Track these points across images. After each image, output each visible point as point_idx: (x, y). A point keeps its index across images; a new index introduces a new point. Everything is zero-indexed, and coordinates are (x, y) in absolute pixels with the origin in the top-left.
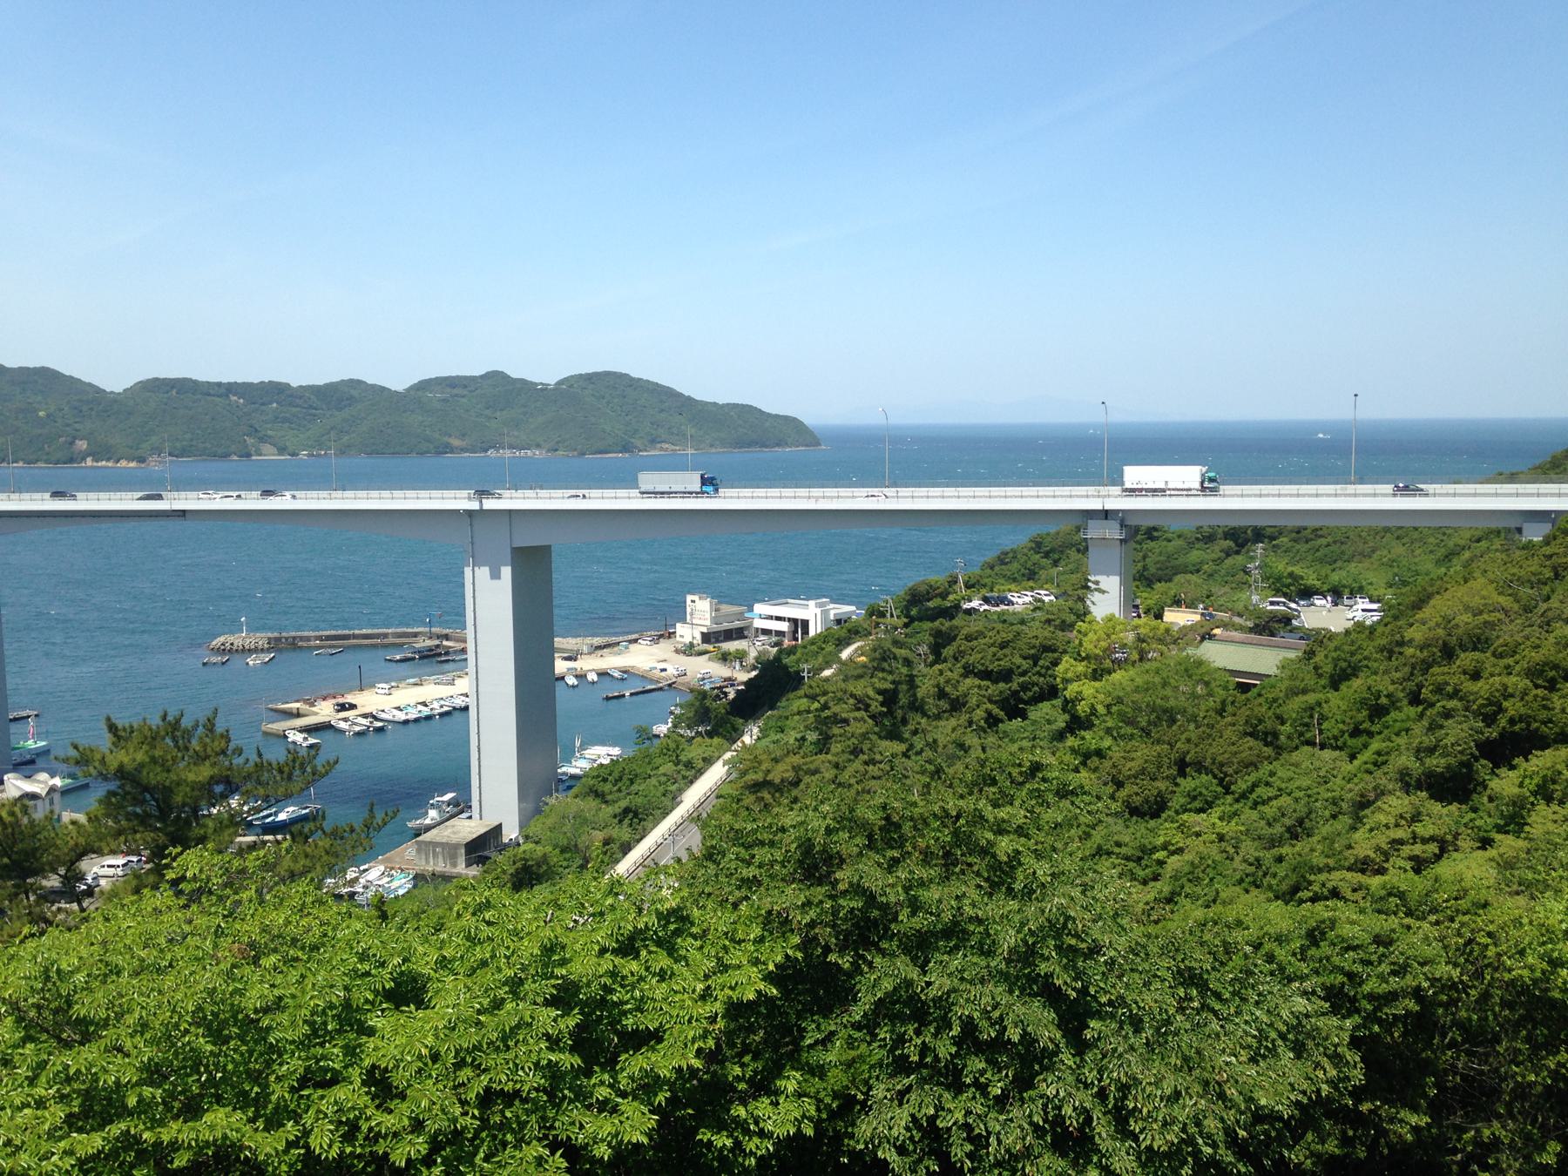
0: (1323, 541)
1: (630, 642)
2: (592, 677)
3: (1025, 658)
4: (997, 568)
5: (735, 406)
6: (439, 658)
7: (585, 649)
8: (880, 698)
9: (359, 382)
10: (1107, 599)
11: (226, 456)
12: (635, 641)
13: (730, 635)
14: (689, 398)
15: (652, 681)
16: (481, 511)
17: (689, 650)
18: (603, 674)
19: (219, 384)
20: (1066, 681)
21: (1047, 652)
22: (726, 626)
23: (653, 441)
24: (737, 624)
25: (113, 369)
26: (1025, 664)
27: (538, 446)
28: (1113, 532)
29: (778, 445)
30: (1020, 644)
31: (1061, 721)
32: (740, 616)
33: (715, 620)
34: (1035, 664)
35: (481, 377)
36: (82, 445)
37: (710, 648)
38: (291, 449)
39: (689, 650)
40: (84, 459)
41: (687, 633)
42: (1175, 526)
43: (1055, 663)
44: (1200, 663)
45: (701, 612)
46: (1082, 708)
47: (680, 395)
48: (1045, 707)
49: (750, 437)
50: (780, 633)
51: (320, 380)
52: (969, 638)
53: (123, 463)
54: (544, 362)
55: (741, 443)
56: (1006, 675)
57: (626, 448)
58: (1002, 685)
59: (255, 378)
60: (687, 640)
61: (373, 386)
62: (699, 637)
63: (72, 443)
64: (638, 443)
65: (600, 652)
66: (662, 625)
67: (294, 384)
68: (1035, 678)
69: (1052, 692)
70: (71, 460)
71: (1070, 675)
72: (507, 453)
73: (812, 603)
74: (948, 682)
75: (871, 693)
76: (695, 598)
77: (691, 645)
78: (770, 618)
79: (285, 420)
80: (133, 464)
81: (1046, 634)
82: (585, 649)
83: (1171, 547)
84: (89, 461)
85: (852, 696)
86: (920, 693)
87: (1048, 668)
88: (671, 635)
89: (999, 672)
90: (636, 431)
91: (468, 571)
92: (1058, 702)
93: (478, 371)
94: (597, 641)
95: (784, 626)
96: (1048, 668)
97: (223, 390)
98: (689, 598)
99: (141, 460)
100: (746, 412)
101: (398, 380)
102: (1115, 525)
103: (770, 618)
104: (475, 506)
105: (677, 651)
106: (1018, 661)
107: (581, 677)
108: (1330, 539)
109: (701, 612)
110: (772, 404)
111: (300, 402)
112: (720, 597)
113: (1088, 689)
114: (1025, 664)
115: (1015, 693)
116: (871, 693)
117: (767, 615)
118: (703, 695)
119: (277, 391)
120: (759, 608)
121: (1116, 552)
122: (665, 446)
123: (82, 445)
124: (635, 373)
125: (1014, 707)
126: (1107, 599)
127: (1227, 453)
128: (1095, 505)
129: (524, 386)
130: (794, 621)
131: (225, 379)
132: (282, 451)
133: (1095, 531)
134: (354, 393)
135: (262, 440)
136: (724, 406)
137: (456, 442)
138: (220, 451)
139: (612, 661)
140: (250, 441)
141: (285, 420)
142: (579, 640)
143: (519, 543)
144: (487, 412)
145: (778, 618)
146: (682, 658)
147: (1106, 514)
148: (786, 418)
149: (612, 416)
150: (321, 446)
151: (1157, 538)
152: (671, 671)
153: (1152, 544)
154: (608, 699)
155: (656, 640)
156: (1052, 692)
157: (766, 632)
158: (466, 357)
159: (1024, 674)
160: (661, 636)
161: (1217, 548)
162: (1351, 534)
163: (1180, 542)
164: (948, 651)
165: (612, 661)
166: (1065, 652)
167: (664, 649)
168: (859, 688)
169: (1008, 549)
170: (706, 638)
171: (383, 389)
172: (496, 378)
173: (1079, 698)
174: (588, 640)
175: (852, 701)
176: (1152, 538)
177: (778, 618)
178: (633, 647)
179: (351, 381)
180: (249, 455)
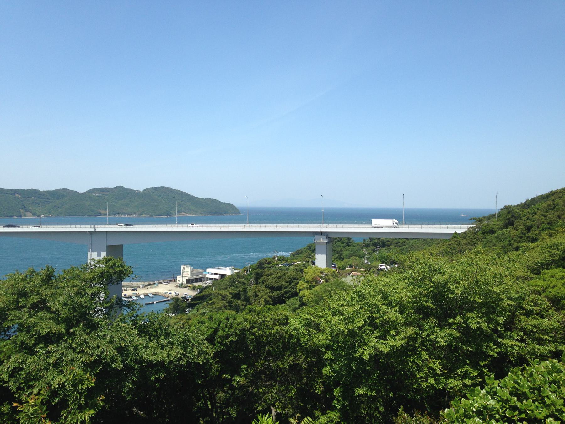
0: (405, 247)
1: (159, 283)
2: (142, 296)
3: (286, 282)
4: (296, 256)
5: (210, 199)
7: (141, 286)
8: (231, 296)
9: (67, 190)
10: (321, 261)
11: (12, 216)
12: (161, 283)
13: (197, 280)
14: (193, 196)
15: (165, 297)
16: (95, 232)
17: (181, 286)
18: (146, 295)
19: (12, 190)
20: (300, 290)
21: (294, 280)
22: (196, 277)
24: (200, 276)
25: (81, 186)
26: (287, 284)
27: (135, 213)
28: (324, 239)
29: (225, 214)
30: (285, 277)
31: (298, 304)
32: (201, 273)
33: (192, 275)
34: (290, 284)
35: (115, 188)
37: (189, 285)
38: (38, 214)
39: (181, 286)
41: (180, 280)
42: (357, 240)
43: (297, 284)
44: (342, 283)
45: (187, 272)
46: (304, 299)
47: (189, 195)
48: (293, 300)
49: (215, 209)
50: (216, 279)
51: (52, 189)
52: (268, 275)
54: (138, 183)
55: (211, 213)
56: (279, 288)
57: (168, 214)
58: (278, 292)
59: (26, 188)
60: (181, 282)
61: (72, 191)
62: (185, 281)
65: (146, 287)
66: (171, 275)
67: (41, 190)
68: (290, 289)
69: (296, 294)
71: (301, 288)
72: (123, 216)
73: (227, 268)
74: (258, 291)
75: (228, 294)
76: (185, 267)
77: (182, 284)
78: (212, 274)
79: (36, 203)
81: (294, 273)
82: (141, 286)
83: (355, 248)
85: (221, 295)
86: (248, 295)
87: (294, 286)
88: (175, 281)
89: (277, 287)
91: (89, 254)
92: (297, 298)
93: (113, 186)
94: (146, 283)
95: (217, 277)
96: (294, 286)
97: (13, 192)
98: (182, 267)
100: (214, 201)
101: (82, 189)
102: (324, 237)
103: (212, 274)
104: (93, 230)
105: (176, 286)
106: (284, 283)
107: (138, 296)
108: (407, 246)
109: (187, 272)
110: (223, 199)
111: (43, 197)
112: (194, 266)
113: (307, 293)
114: (287, 284)
115: (283, 295)
116: (228, 294)
117: (212, 273)
118: (177, 299)
119: (34, 193)
120: (209, 270)
121: (325, 247)
122: (183, 213)
124: (173, 187)
125: (280, 301)
126: (321, 261)
128: (318, 230)
129: (131, 191)
130: (221, 275)
131: (14, 188)
132: (34, 214)
133: (319, 239)
134: (65, 193)
135: (26, 211)
136: (206, 199)
137: (102, 212)
139: (151, 291)
140: (22, 211)
141: (36, 203)
142: (139, 283)
143: (108, 244)
144: (116, 201)
145: (215, 274)
146: (178, 289)
147: (322, 233)
148: (228, 204)
149: (164, 201)
150: (50, 213)
151: (350, 245)
152: (173, 293)
153: (349, 247)
154: (147, 304)
155: (169, 282)
156: (296, 294)
157: (211, 279)
158: (109, 181)
159: (286, 288)
160: (171, 281)
161: (370, 249)
162: (414, 244)
163: (358, 247)
164: (260, 280)
165: (151, 291)
166: (300, 280)
167: (172, 285)
168: (223, 292)
169: (299, 249)
170: (188, 281)
171: (76, 192)
172: (120, 189)
173: (304, 296)
174: (143, 283)
175: (220, 297)
176: (349, 245)
177: (215, 274)
178: (160, 285)
179: (64, 189)
180: (21, 216)
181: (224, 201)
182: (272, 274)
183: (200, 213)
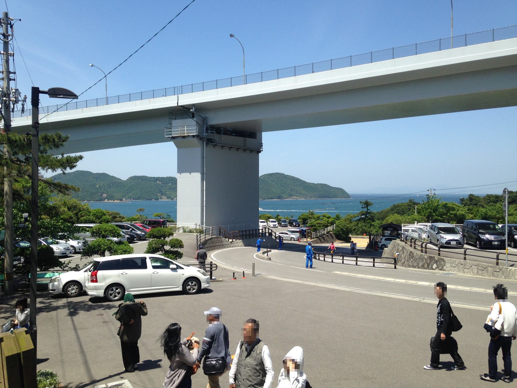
6: (145, 258)
11: (151, 199)
14: (304, 182)
19: (154, 178)
23: (290, 196)
36: (105, 195)
40: (105, 200)
47: (301, 180)
53: (116, 201)
55: (321, 197)
57: (279, 198)
59: (165, 175)
63: (102, 195)
64: (285, 196)
70: (101, 200)
80: (118, 201)
84: (106, 201)
90: (284, 192)
99: (121, 200)
100: (324, 187)
122: (294, 197)
123: (105, 195)
127: (363, 238)
132: (168, 198)
135: (162, 194)
138: (149, 198)
140: (159, 195)
148: (338, 188)
180: (158, 199)
181: (334, 186)
182: (128, 228)
183: (311, 197)
